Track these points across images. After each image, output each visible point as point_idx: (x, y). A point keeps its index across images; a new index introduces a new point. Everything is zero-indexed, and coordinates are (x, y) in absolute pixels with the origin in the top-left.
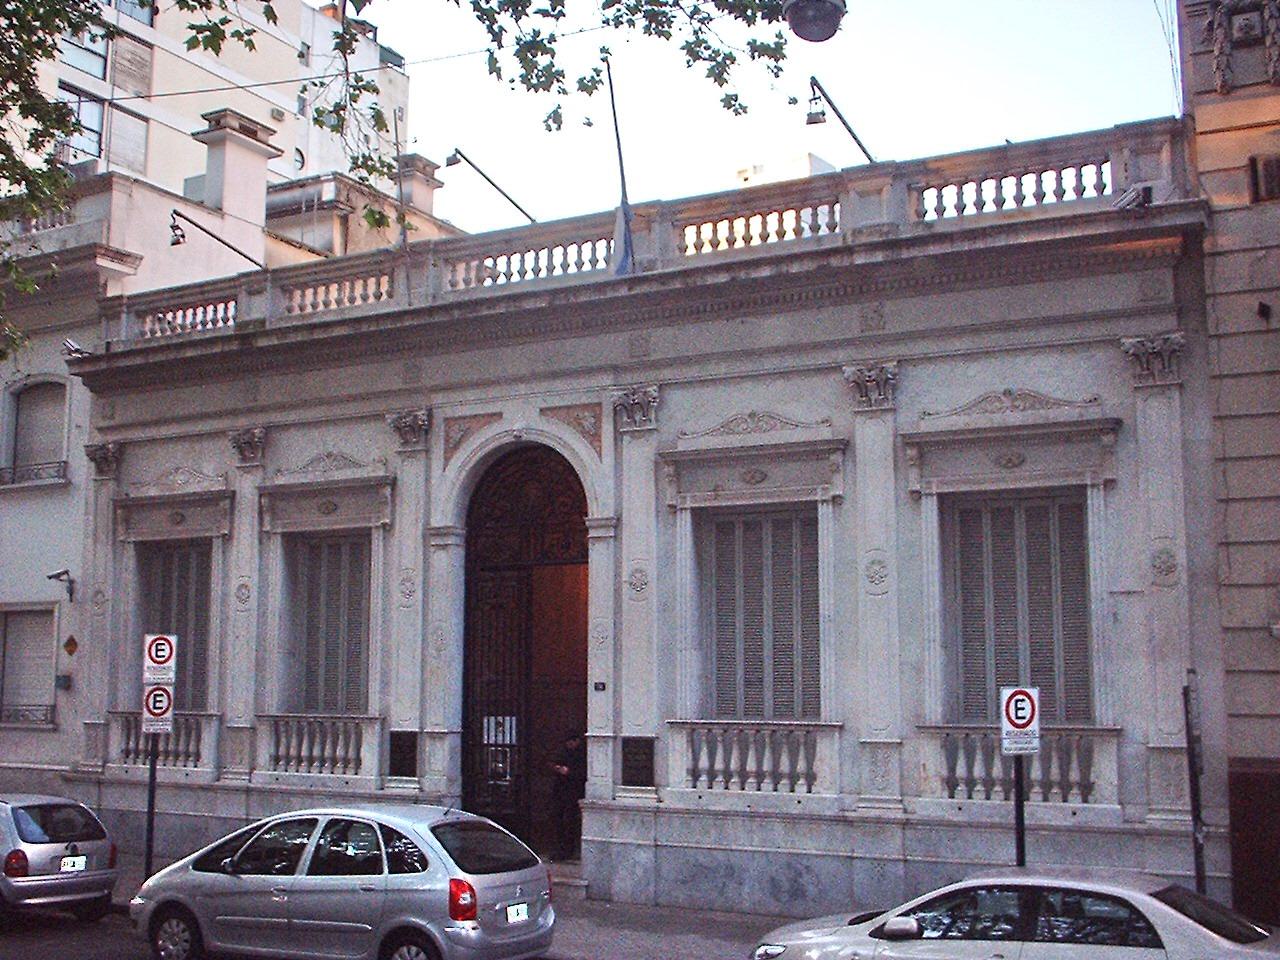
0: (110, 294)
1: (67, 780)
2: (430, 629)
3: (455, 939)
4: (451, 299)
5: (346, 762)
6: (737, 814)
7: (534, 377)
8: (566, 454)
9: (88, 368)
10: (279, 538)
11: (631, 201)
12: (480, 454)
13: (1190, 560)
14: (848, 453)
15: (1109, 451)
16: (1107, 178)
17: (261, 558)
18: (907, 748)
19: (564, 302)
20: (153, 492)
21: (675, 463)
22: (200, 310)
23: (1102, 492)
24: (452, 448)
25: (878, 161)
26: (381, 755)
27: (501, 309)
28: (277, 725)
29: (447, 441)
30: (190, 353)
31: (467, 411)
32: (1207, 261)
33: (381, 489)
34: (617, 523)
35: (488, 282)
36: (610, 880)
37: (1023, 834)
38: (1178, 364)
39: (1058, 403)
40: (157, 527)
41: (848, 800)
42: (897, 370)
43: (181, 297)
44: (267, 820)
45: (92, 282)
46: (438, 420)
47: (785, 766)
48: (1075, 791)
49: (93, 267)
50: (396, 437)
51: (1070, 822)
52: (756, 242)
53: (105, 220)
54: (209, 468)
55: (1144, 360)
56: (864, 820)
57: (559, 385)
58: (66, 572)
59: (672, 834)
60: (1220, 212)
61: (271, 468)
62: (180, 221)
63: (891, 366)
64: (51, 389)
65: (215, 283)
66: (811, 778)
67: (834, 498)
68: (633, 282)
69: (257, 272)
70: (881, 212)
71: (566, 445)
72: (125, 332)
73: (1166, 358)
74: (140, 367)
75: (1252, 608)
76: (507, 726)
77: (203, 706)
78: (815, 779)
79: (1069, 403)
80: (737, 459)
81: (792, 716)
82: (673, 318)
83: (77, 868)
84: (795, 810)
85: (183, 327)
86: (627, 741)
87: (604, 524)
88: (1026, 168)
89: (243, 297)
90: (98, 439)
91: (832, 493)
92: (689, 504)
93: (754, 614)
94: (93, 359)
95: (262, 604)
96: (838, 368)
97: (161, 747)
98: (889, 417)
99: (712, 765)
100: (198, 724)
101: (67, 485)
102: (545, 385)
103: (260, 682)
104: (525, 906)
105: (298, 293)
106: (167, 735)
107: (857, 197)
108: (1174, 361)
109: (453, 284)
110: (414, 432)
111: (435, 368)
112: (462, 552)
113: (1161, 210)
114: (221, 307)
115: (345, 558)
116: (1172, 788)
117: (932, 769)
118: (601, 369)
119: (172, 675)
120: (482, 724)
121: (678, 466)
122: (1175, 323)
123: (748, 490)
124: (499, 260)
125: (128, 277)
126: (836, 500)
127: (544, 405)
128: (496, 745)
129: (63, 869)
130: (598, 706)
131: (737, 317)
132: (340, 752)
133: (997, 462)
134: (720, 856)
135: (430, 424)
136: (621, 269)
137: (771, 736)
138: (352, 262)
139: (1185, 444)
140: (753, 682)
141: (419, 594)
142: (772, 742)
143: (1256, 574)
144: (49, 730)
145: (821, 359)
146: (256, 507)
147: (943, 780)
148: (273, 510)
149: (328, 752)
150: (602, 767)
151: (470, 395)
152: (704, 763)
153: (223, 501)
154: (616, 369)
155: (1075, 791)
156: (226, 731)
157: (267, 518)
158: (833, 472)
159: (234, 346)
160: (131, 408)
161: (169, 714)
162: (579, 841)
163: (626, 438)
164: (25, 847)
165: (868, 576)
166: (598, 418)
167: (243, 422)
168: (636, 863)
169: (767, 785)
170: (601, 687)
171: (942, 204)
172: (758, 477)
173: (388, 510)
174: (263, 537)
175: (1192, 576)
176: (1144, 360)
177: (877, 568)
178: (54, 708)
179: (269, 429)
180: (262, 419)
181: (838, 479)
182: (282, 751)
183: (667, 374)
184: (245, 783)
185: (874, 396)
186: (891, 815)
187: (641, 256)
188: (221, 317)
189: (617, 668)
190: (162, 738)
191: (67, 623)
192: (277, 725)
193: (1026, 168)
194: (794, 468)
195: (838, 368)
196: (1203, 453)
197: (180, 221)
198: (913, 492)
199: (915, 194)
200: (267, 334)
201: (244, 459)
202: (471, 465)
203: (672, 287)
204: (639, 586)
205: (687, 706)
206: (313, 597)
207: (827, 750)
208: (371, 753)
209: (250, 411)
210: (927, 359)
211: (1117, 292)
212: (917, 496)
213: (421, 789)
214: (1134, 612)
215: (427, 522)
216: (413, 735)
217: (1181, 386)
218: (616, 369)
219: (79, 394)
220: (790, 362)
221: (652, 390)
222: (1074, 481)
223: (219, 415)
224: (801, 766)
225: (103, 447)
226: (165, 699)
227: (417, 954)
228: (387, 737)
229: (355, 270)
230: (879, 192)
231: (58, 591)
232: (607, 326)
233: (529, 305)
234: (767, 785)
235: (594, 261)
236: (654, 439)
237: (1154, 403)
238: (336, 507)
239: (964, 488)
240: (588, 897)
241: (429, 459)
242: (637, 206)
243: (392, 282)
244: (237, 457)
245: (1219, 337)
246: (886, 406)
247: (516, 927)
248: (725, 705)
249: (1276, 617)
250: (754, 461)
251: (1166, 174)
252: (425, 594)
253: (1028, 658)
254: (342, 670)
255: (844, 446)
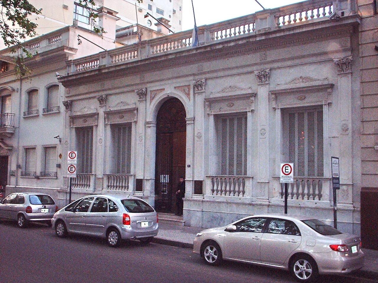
0: (69, 59)
1: (59, 192)
2: (146, 150)
3: (125, 230)
4: (152, 56)
5: (125, 187)
6: (223, 202)
7: (173, 78)
8: (181, 100)
9: (63, 80)
10: (109, 125)
11: (197, 26)
12: (160, 100)
13: (353, 127)
14: (256, 97)
15: (330, 94)
16: (191, 42)
17: (105, 131)
18: (271, 183)
19: (179, 56)
20: (79, 114)
21: (275, 94)
22: (130, 54)
23: (328, 106)
24: (152, 99)
25: (175, 33)
26: (134, 185)
27: (163, 59)
28: (109, 177)
29: (150, 98)
30: (87, 75)
31: (155, 89)
32: (360, 34)
33: (133, 111)
34: (194, 119)
35: (184, 46)
36: (190, 220)
37: (287, 209)
38: (351, 66)
39: (315, 80)
40: (80, 124)
41: (254, 199)
42: (269, 72)
43: (86, 60)
44: (80, 199)
45: (65, 56)
46: (149, 90)
47: (237, 189)
48: (317, 197)
49: (64, 53)
50: (138, 96)
51: (314, 206)
52: (242, 33)
53: (68, 39)
54: (92, 107)
55: (341, 66)
56: (257, 205)
57: (179, 80)
58: (59, 136)
59: (206, 208)
60: (363, 18)
61: (107, 107)
62: (80, 38)
63: (267, 70)
64: (55, 86)
65: (94, 55)
66: (244, 192)
67: (252, 110)
68: (197, 49)
69: (104, 52)
70: (267, 25)
71: (181, 97)
72: (72, 70)
73: (347, 65)
74: (75, 79)
75: (370, 141)
76: (166, 177)
77: (130, 172)
78: (322, 196)
79: (319, 80)
80: (225, 100)
81: (241, 175)
82: (209, 59)
83: (45, 212)
84: (239, 201)
85: (86, 68)
86: (196, 181)
87: (191, 119)
88: (291, 13)
89: (101, 59)
90: (66, 100)
91: (251, 109)
92: (213, 113)
93: (301, 143)
94: (64, 77)
95: (105, 143)
96: (252, 72)
97: (289, 190)
98: (267, 86)
99: (303, 191)
100: (90, 177)
101: (59, 113)
102: (174, 81)
103: (105, 165)
104: (148, 222)
105: (114, 57)
106: (75, 178)
107: (260, 20)
108: (350, 65)
109: (153, 52)
110: (142, 95)
111: (148, 76)
112: (155, 128)
113: (348, 18)
114: (96, 62)
115: (236, 122)
116: (345, 196)
117: (276, 190)
118: (191, 75)
119: (76, 162)
120: (160, 177)
121: (210, 102)
122: (350, 53)
123: (229, 108)
124: (187, 40)
125: (74, 55)
126: (252, 111)
127: (176, 86)
128: (164, 183)
129: (42, 212)
130: (188, 171)
131: (226, 58)
132: (118, 184)
133: (298, 98)
134: (219, 214)
135: (146, 92)
136: (194, 45)
137: (318, 182)
138: (127, 48)
139: (352, 91)
140: (231, 165)
141: (143, 140)
142: (307, 184)
143: (372, 131)
144: (55, 179)
145: (249, 69)
146: (104, 117)
147: (280, 193)
148: (108, 118)
149: (300, 191)
150: (189, 188)
151: (157, 84)
152: (215, 188)
153: (95, 116)
154: (194, 75)
155: (317, 197)
156: (96, 179)
157: (106, 120)
158: (252, 103)
159: (97, 73)
160: (75, 91)
161: (75, 173)
162: (182, 210)
163: (197, 95)
164: (31, 205)
165: (342, 129)
166: (189, 89)
167: (100, 94)
168: (197, 216)
169: (232, 194)
170: (189, 166)
171: (284, 21)
172: (303, 98)
173: (136, 117)
174: (106, 125)
175: (353, 132)
176: (341, 66)
177: (263, 131)
178: (57, 172)
179: (107, 95)
180: (105, 93)
181: (253, 105)
182: (110, 184)
183: (208, 76)
184: (202, 199)
185: (263, 80)
186: (264, 203)
187: (201, 41)
188: (95, 65)
189: (193, 161)
190: (72, 179)
191: (59, 150)
192: (109, 177)
193: (297, 11)
194: (240, 102)
195: (252, 72)
196: (358, 94)
197: (80, 38)
198: (273, 108)
199: (277, 19)
200: (105, 69)
201: (101, 104)
202: (156, 104)
203: (193, 53)
204: (199, 137)
205: (213, 171)
206: (224, 137)
207: (249, 184)
208: (131, 185)
209: (103, 90)
210: (279, 68)
211: (333, 46)
212: (274, 109)
213: (144, 195)
214: (336, 143)
215: (146, 120)
216: (142, 179)
217: (352, 73)
218: (194, 75)
219: (62, 88)
220: (88, 96)
221: (203, 81)
222: (319, 104)
223: (94, 92)
224: (241, 189)
225: (67, 102)
226: (74, 169)
227: (115, 234)
228: (135, 180)
229: (128, 50)
230: (266, 18)
231: (57, 141)
232: (192, 63)
233: (170, 57)
234: (232, 194)
235: (249, 30)
236: (204, 94)
237: (343, 79)
238: (123, 117)
239: (288, 106)
240: (185, 225)
241: (146, 103)
242: (198, 27)
243: (137, 52)
244: (99, 103)
245: (363, 57)
246: (266, 83)
247: (144, 228)
248: (223, 171)
249: (377, 144)
250: (230, 100)
251: (349, 7)
252: (145, 139)
253: (307, 158)
254: (126, 161)
255: (255, 95)
